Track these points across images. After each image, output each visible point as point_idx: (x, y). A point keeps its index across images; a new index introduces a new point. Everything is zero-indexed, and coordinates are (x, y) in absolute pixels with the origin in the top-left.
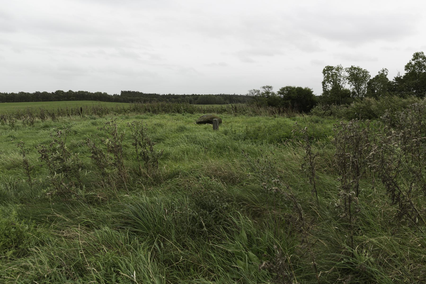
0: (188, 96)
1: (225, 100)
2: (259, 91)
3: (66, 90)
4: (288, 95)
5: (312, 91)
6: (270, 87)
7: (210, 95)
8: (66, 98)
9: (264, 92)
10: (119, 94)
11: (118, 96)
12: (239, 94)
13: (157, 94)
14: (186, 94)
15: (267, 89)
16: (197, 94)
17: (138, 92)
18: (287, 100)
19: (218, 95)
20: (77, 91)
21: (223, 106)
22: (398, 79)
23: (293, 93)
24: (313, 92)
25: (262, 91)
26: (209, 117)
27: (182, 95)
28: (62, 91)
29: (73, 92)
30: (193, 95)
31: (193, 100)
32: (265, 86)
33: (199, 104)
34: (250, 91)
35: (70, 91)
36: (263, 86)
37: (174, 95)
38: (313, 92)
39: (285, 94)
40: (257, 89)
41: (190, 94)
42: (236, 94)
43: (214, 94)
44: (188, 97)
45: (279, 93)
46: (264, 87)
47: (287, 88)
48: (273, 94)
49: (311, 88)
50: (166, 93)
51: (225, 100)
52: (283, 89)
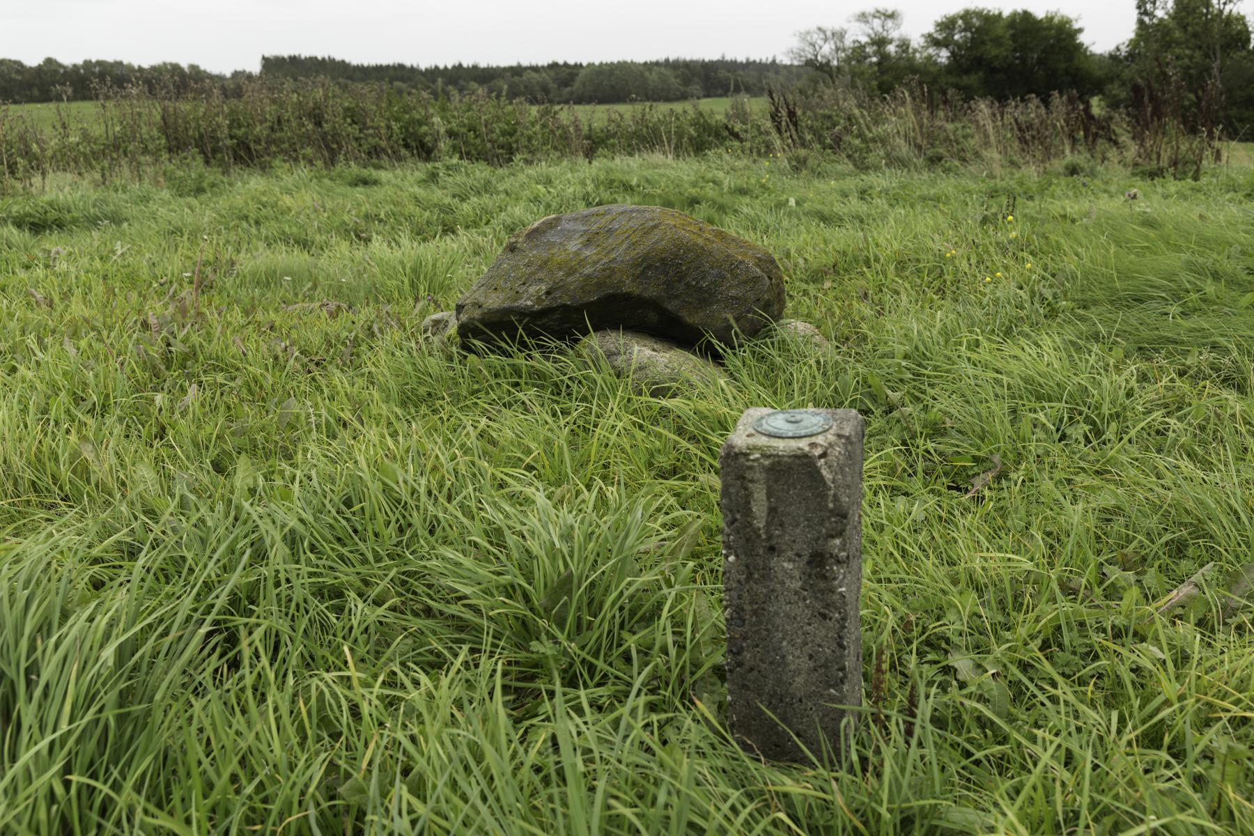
0: (535, 69)
1: (687, 82)
2: (839, 35)
3: (32, 60)
4: (968, 49)
5: (1076, 26)
6: (892, 16)
7: (623, 66)
8: (36, 92)
9: (864, 40)
10: (255, 68)
11: (249, 77)
12: (741, 58)
13: (408, 64)
14: (525, 63)
15: (877, 23)
16: (571, 62)
17: (332, 61)
18: (967, 71)
19: (657, 64)
20: (80, 62)
21: (678, 107)
22: (1081, 45)
23: (997, 41)
24: (1080, 30)
25: (858, 34)
26: (621, 253)
27: (511, 69)
28: (19, 64)
29: (61, 66)
30: (554, 66)
31: (553, 86)
32: (870, 9)
33: (579, 101)
34: (804, 36)
35: (49, 61)
36: (858, 10)
37: (475, 67)
38: (1080, 30)
39: (957, 43)
40: (832, 24)
41: (543, 60)
42: (728, 58)
43: (640, 58)
44: (535, 75)
45: (934, 42)
46: (863, 17)
47: (967, 16)
48: (904, 45)
49: (1072, 16)
50: (446, 61)
51: (687, 82)
52: (947, 25)
